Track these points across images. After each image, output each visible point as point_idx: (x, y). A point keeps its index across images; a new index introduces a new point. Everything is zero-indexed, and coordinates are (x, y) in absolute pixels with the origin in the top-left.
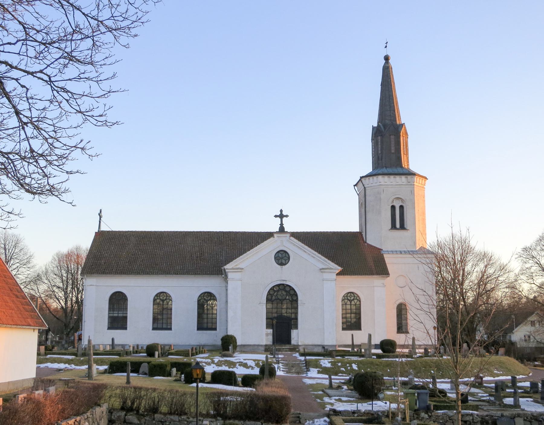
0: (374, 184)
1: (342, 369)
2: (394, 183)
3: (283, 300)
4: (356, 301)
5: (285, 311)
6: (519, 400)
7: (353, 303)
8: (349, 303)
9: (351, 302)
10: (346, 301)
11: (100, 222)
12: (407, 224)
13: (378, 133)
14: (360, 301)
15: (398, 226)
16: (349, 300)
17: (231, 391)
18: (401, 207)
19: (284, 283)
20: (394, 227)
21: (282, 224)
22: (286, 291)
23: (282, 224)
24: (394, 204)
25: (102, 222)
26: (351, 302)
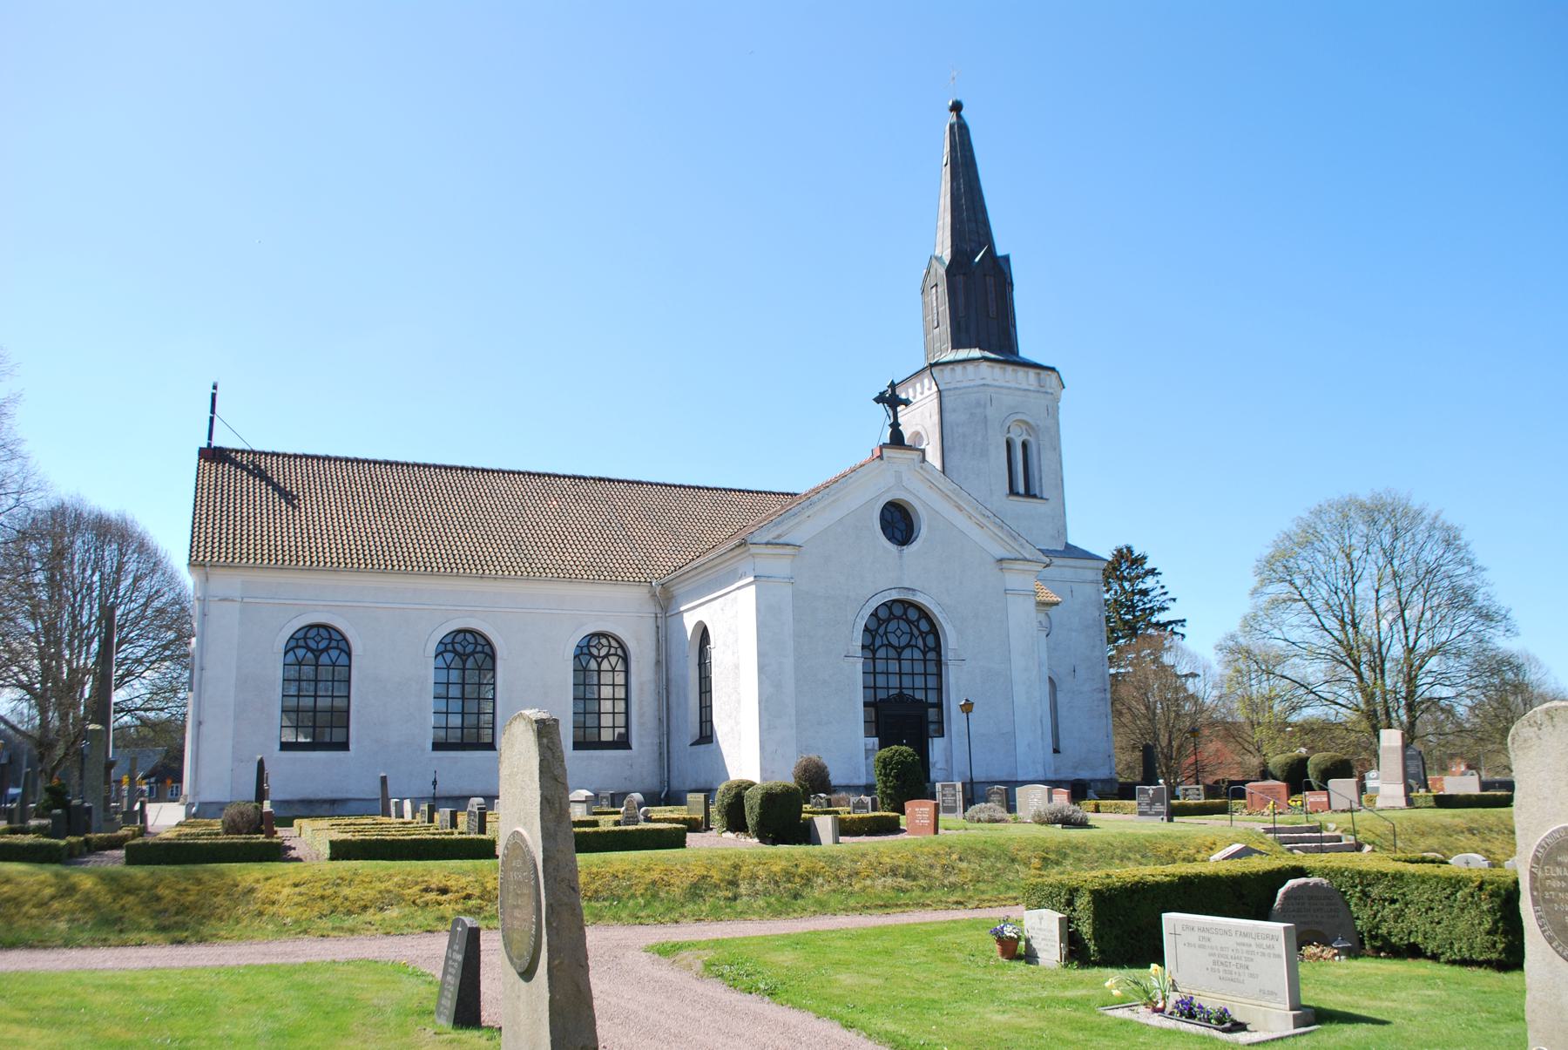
0: (965, 384)
1: (91, 727)
2: (1013, 384)
3: (904, 648)
4: (334, 653)
5: (907, 679)
6: (574, 860)
7: (324, 659)
8: (457, 662)
9: (317, 658)
10: (301, 652)
11: (212, 420)
12: (1046, 486)
13: (959, 269)
14: (349, 655)
15: (1021, 490)
16: (312, 651)
17: (765, 938)
18: (1025, 445)
19: (909, 597)
20: (1013, 491)
21: (895, 426)
22: (908, 622)
23: (895, 426)
24: (1011, 435)
25: (216, 420)
26: (317, 658)
